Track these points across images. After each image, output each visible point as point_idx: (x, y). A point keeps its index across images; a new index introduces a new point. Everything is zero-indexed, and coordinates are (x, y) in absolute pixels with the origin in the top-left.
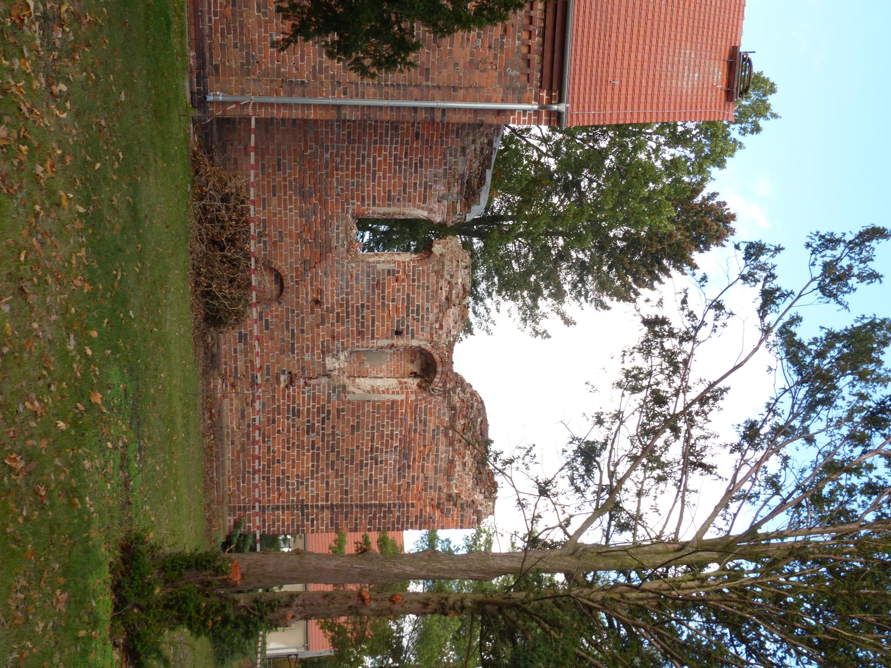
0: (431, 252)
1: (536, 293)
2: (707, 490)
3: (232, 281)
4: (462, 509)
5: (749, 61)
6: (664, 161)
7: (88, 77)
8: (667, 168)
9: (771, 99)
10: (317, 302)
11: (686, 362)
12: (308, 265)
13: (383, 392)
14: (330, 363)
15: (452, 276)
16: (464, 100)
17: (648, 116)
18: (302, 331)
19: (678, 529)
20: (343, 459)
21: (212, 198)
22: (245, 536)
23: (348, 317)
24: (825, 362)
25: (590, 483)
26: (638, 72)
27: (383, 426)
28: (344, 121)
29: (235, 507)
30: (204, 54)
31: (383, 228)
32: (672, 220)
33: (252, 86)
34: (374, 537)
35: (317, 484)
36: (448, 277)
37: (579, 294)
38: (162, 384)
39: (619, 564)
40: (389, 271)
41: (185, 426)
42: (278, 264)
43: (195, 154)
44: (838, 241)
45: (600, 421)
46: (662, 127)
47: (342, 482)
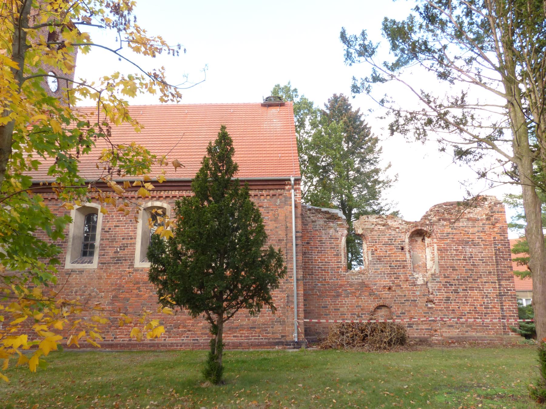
0: (362, 234)
1: (376, 182)
2: (475, 94)
3: (382, 331)
4: (494, 212)
5: (267, 98)
6: (312, 129)
7: (294, 403)
8: (315, 128)
9: (282, 86)
10: (390, 288)
11: (411, 113)
12: (371, 293)
13: (433, 255)
14: (420, 282)
15: (373, 224)
16: (291, 223)
17: (293, 140)
18: (405, 296)
19: (500, 106)
20: (471, 275)
21: (342, 340)
22: (521, 326)
23: (396, 274)
24: (405, 47)
25: (477, 152)
26: (275, 146)
27: (452, 255)
28: (303, 277)
29: (504, 332)
30: (277, 342)
31: (350, 255)
32: (338, 122)
33: (290, 320)
34: (514, 256)
35: (486, 288)
36: (373, 226)
37: (375, 161)
38: (440, 371)
39: (524, 135)
40: (372, 254)
41: (461, 358)
42: (372, 308)
43: (322, 348)
44: (348, 52)
45: (443, 150)
46: (297, 132)
47: (484, 275)
